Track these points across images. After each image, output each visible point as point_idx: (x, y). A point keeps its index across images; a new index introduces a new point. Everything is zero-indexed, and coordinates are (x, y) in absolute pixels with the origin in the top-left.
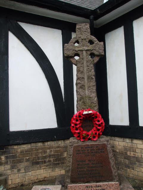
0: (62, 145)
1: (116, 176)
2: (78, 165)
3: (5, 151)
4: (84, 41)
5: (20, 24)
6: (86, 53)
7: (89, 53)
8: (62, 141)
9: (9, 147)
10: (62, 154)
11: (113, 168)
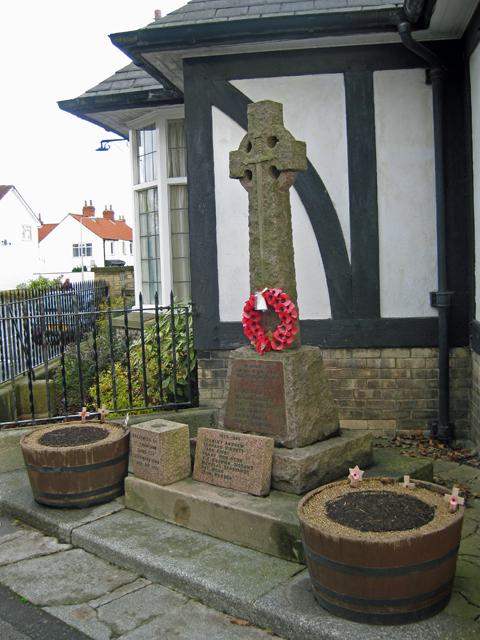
0: (345, 361)
1: (291, 430)
2: (237, 397)
3: (212, 361)
4: (259, 142)
5: (237, 87)
6: (263, 167)
7: (267, 166)
8: (345, 351)
9: (220, 354)
10: (343, 381)
11: (289, 413)
